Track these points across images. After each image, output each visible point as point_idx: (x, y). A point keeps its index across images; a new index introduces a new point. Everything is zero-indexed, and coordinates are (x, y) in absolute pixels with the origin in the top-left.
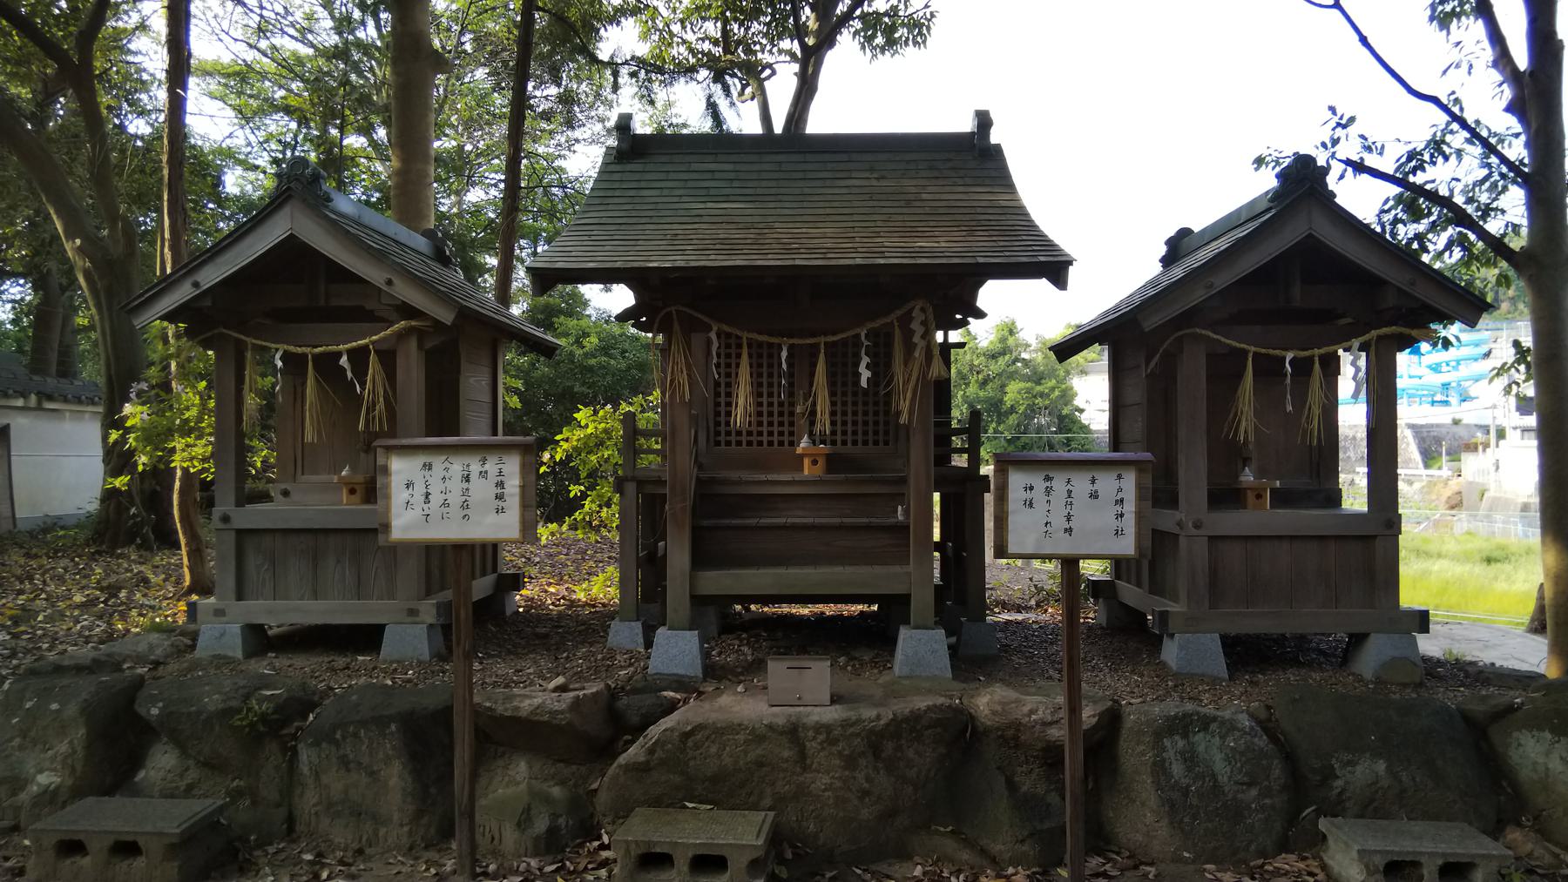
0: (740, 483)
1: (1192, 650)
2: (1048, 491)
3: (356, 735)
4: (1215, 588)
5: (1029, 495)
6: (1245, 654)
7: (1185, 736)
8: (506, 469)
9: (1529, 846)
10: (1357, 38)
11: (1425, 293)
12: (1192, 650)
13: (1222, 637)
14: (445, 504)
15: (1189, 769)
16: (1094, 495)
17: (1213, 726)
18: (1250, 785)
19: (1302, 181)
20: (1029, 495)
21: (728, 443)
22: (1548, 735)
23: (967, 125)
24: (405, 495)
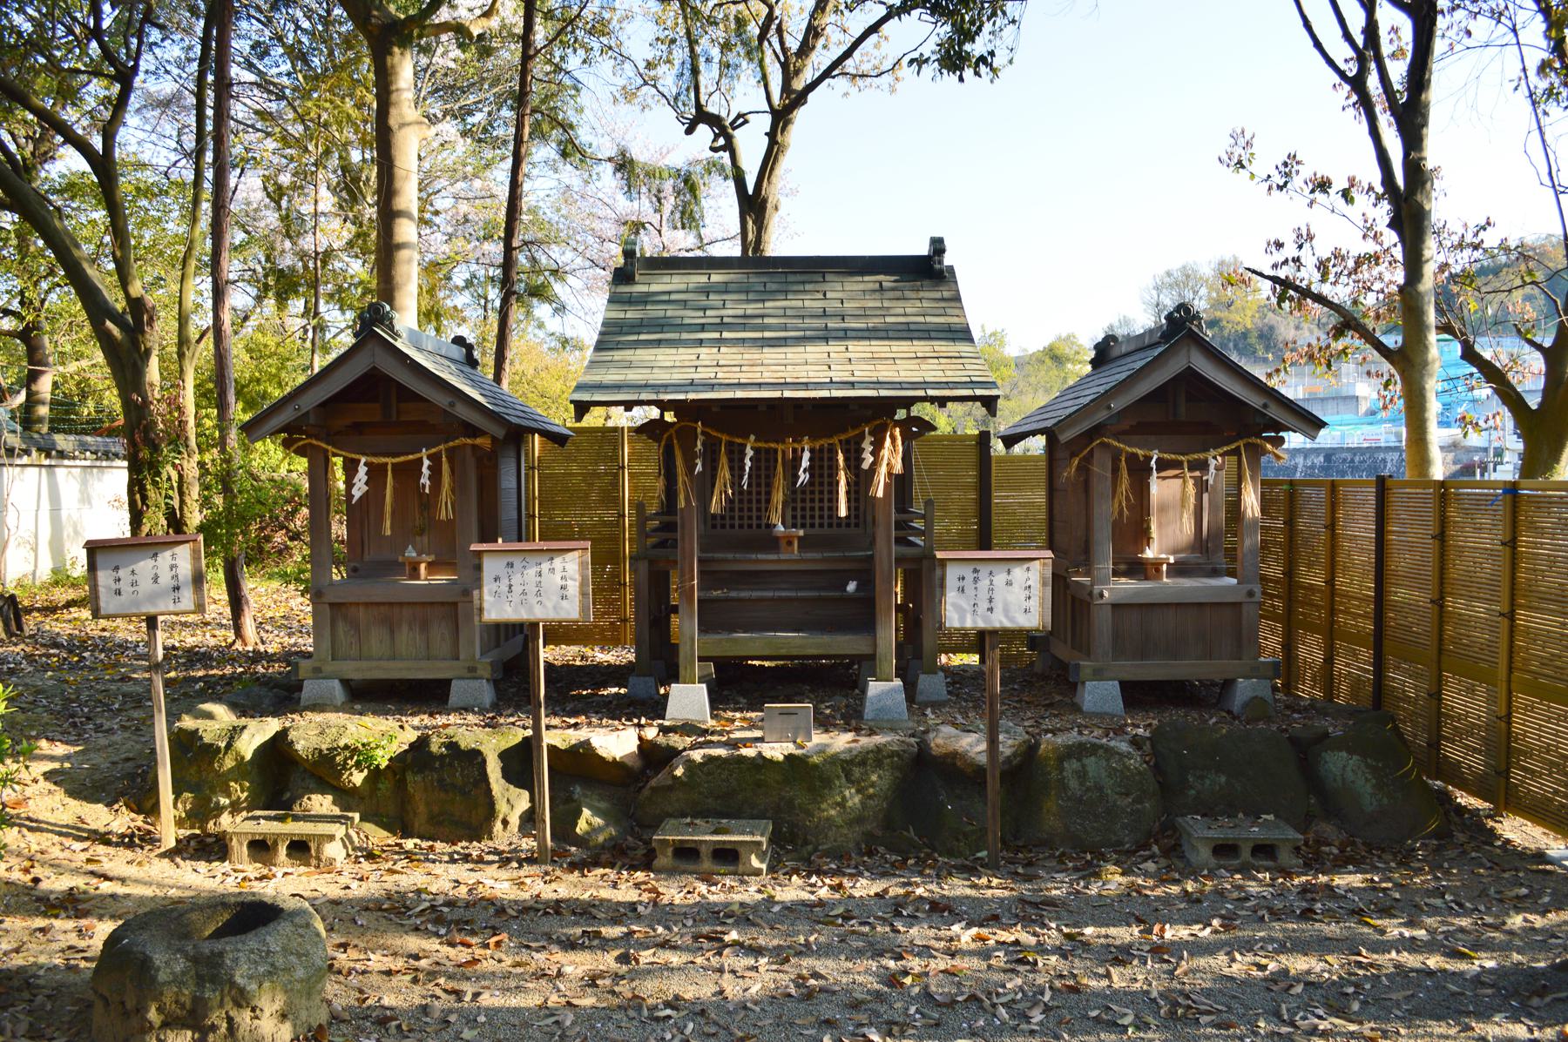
0: (727, 561)
1: (1100, 694)
2: (976, 580)
3: (451, 765)
4: (1120, 647)
5: (961, 584)
6: (1137, 695)
7: (1079, 760)
8: (568, 566)
9: (844, 702)
10: (1340, 32)
11: (1274, 412)
12: (1100, 694)
13: (1121, 683)
14: (524, 593)
15: (1081, 784)
16: (1009, 583)
17: (1101, 752)
18: (1127, 795)
19: (1180, 326)
20: (961, 584)
21: (723, 526)
22: (1344, 754)
23: (923, 249)
24: (494, 586)
